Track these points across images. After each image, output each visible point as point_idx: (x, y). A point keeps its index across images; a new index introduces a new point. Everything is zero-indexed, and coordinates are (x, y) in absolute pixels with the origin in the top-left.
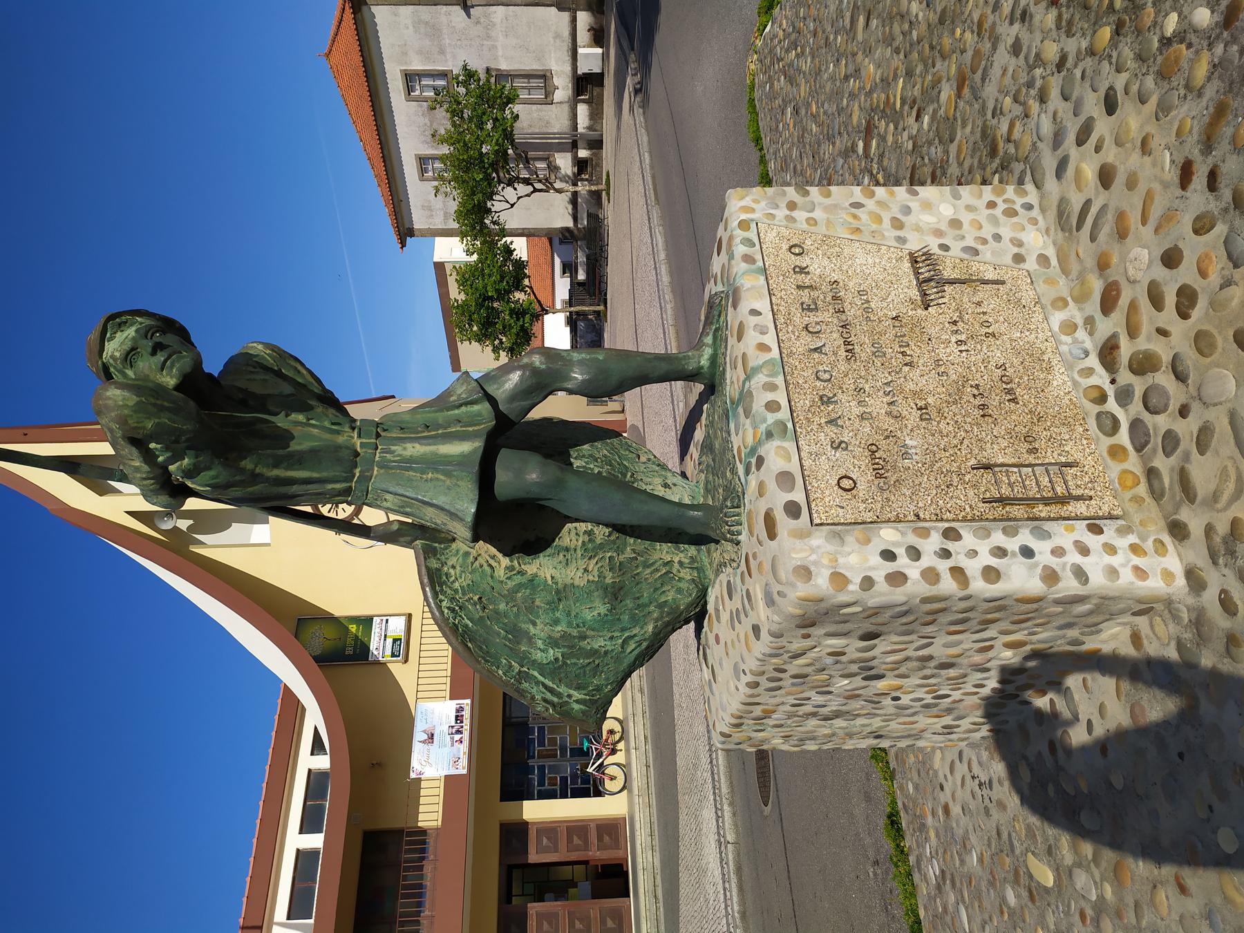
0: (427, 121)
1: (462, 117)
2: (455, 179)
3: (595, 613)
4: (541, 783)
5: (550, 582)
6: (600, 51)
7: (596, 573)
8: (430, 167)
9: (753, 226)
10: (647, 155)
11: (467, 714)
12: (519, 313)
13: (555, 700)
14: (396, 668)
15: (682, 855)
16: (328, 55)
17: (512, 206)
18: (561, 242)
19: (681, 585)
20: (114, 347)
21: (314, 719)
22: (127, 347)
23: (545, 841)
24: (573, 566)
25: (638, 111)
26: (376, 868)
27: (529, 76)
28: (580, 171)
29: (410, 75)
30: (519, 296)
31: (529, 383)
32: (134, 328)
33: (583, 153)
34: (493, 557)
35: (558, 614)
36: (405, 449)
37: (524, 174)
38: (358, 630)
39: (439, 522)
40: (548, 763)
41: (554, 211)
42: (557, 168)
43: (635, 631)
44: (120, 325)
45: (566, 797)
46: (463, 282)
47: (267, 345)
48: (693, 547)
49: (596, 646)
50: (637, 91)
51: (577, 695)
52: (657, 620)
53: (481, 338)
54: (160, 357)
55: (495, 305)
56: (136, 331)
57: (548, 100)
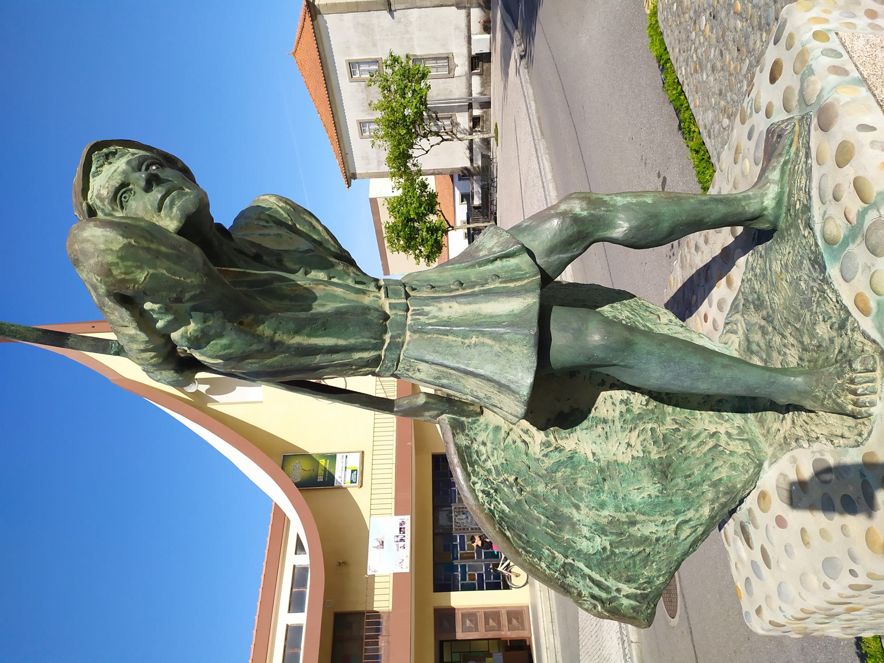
0: (365, 96)
1: (390, 91)
2: (387, 134)
3: (645, 495)
4: (464, 578)
5: (591, 459)
6: (487, 36)
7: (640, 448)
8: (367, 129)
9: (832, 36)
10: (533, 103)
11: (407, 527)
12: (433, 230)
13: (604, 595)
14: (354, 491)
15: (582, 643)
16: (294, 54)
17: (427, 152)
18: (460, 179)
19: (734, 460)
20: (102, 183)
21: (296, 528)
22: (116, 182)
23: (468, 622)
24: (613, 440)
25: (523, 71)
26: (346, 645)
27: (436, 59)
28: (474, 126)
29: (352, 63)
30: (433, 218)
31: (570, 232)
32: (124, 160)
33: (477, 112)
34: (526, 432)
35: (604, 497)
36: (440, 309)
37: (434, 129)
38: (326, 463)
39: (481, 395)
40: (468, 563)
41: (454, 155)
42: (458, 124)
43: (690, 514)
44: (107, 156)
45: (482, 589)
46: (392, 210)
47: (281, 199)
48: (738, 415)
49: (647, 533)
50: (522, 57)
51: (627, 589)
52: (713, 501)
53: (406, 248)
54: (157, 193)
55: (416, 224)
56: (128, 163)
57: (450, 75)
